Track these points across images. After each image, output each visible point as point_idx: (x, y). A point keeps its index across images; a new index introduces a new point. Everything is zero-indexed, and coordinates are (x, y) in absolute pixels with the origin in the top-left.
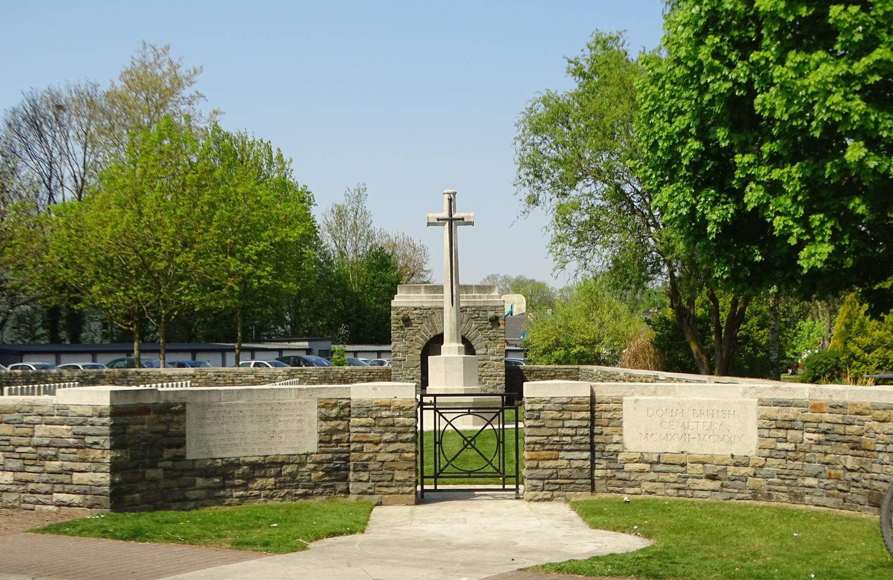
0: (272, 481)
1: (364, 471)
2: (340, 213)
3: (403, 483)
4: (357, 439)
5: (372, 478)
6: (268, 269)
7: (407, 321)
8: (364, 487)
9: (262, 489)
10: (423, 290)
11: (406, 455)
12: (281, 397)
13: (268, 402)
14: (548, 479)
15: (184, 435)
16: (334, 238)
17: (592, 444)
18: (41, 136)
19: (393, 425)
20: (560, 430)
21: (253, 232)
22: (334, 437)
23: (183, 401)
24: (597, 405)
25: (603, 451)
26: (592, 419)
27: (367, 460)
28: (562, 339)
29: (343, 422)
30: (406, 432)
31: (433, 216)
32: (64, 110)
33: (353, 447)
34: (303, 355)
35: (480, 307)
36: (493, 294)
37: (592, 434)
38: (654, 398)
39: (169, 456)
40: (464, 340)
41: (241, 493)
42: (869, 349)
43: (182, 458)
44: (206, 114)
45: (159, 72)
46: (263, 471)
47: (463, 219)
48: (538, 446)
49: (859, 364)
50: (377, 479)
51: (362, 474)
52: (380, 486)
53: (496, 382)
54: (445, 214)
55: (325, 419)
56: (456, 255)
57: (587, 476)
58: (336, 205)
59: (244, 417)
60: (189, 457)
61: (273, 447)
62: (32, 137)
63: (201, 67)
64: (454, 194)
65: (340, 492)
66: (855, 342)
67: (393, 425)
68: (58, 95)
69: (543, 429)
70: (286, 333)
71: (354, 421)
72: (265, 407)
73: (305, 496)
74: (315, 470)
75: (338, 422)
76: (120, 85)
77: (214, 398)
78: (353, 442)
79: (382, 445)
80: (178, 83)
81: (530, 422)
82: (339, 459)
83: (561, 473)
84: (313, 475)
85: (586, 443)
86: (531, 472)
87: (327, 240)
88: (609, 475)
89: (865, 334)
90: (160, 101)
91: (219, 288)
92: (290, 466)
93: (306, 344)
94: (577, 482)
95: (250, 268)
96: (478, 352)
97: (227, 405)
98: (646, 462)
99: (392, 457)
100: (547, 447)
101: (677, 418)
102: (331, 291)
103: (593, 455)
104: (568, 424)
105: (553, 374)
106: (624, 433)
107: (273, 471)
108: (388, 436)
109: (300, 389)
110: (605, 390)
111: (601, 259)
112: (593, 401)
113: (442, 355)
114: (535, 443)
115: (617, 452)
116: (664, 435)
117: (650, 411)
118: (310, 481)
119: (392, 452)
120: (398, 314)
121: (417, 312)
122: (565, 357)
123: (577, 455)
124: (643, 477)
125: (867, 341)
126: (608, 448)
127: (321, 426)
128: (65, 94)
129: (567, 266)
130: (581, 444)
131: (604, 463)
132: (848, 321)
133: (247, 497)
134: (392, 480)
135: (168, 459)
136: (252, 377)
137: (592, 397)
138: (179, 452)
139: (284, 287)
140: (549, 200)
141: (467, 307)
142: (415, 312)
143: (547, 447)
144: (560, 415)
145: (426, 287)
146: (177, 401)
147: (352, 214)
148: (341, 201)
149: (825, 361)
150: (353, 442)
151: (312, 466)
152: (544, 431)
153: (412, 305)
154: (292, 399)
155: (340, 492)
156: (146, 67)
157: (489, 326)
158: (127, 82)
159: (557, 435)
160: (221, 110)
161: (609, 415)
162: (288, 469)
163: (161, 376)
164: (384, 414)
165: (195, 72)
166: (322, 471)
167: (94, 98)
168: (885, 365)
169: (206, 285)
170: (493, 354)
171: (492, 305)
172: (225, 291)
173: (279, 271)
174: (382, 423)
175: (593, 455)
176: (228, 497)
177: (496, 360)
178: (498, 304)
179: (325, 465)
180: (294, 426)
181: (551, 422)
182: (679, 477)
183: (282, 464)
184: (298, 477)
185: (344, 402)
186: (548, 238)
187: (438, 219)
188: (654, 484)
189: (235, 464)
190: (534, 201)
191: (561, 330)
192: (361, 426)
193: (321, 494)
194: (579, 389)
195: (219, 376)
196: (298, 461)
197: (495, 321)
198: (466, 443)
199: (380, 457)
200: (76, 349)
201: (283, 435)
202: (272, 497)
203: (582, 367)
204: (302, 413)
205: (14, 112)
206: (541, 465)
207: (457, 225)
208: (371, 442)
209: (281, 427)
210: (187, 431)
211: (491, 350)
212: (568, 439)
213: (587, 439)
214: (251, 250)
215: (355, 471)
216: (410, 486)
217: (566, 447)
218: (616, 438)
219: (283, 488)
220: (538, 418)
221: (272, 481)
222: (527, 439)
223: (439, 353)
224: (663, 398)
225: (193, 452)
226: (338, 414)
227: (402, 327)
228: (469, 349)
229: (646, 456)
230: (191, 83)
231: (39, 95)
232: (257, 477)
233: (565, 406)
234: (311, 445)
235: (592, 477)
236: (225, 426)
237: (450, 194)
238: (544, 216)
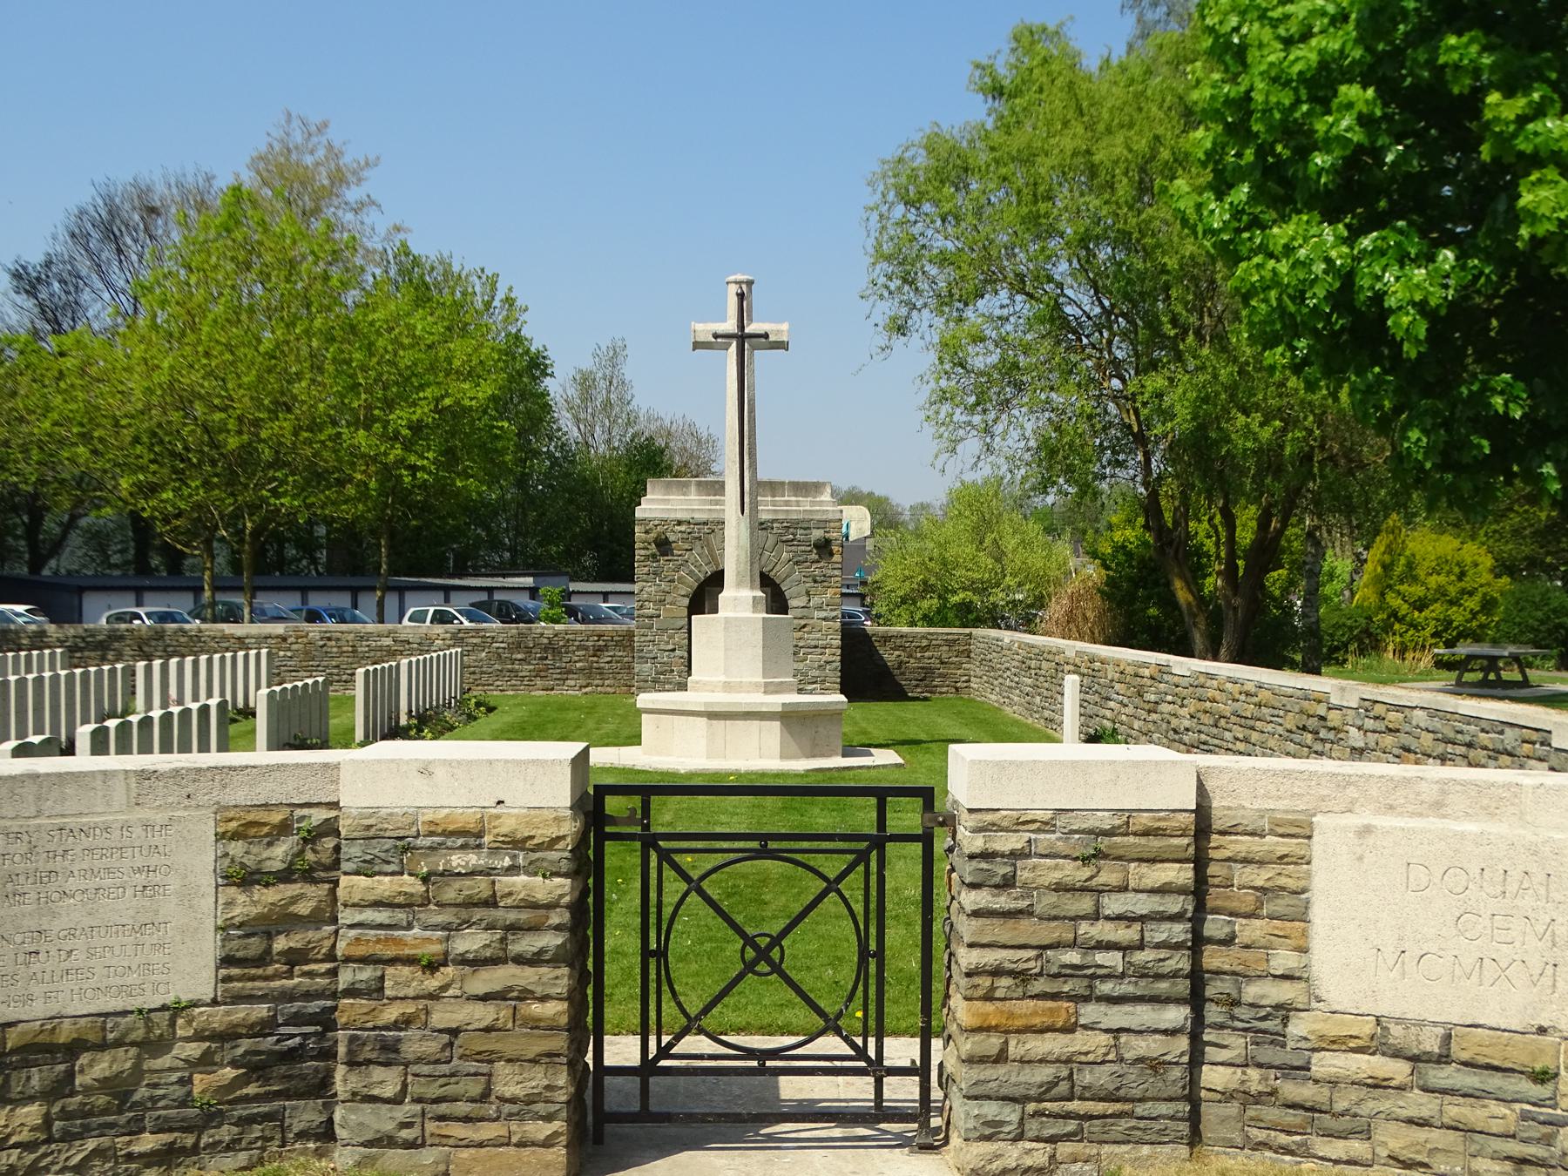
0: (31, 1113)
1: (387, 1064)
2: (585, 383)
3: (525, 1106)
4: (360, 951)
5: (415, 1089)
6: (430, 455)
7: (664, 546)
8: (383, 1120)
10: (693, 488)
11: (536, 1008)
12: (71, 806)
14: (1039, 1100)
16: (578, 421)
17: (1197, 977)
18: (119, 251)
20: (1084, 927)
21: (406, 386)
22: (280, 944)
24: (1216, 839)
25: (1236, 1003)
26: (1199, 889)
27: (395, 1026)
28: (933, 580)
29: (310, 890)
30: (534, 928)
31: (705, 330)
32: (159, 214)
33: (345, 977)
34: (523, 600)
35: (798, 522)
36: (823, 498)
37: (1198, 942)
38: (1433, 823)
40: (767, 582)
42: (1420, 605)
44: (382, 230)
45: (309, 160)
47: (766, 336)
48: (1005, 982)
49: (1404, 628)
50: (434, 1091)
51: (378, 1073)
52: (442, 1118)
53: (824, 658)
54: (730, 326)
55: (247, 878)
56: (752, 410)
57: (1176, 1090)
58: (580, 371)
61: (37, 990)
62: (108, 253)
63: (378, 158)
64: (750, 283)
65: (302, 1135)
66: (1399, 593)
67: (491, 902)
68: (149, 189)
69: (1025, 923)
70: (501, 563)
71: (352, 885)
74: (205, 1062)
76: (248, 179)
78: (348, 959)
79: (450, 970)
80: (339, 178)
81: (982, 899)
82: (297, 1019)
83: (1086, 1077)
84: (200, 1082)
85: (1175, 975)
86: (978, 1073)
87: (565, 422)
88: (1255, 1087)
89: (1415, 579)
90: (309, 205)
91: (341, 483)
92: (106, 1057)
93: (529, 581)
94: (1140, 1110)
95: (398, 451)
96: (792, 603)
98: (1397, 1054)
99: (484, 1014)
100: (1039, 986)
101: (1527, 902)
102: (571, 501)
103: (1198, 1020)
104: (1113, 905)
105: (925, 643)
106: (1317, 944)
107: (36, 1079)
108: (471, 942)
109: (144, 775)
110: (1251, 783)
111: (1021, 430)
112: (1203, 822)
113: (721, 614)
114: (997, 972)
115: (1284, 1011)
116: (1469, 960)
117: (1419, 874)
118: (183, 1103)
119: (485, 998)
120: (647, 532)
121: (683, 528)
122: (939, 611)
123: (1143, 1015)
124: (1385, 1106)
125: (1417, 591)
126: (1251, 992)
127: (230, 904)
128: (160, 189)
129: (959, 448)
130: (1159, 977)
131: (1237, 1045)
132: (1387, 558)
134: (484, 1097)
136: (388, 642)
137: (1202, 812)
139: (459, 484)
140: (929, 325)
141: (773, 521)
142: (678, 528)
143: (1039, 986)
144: (1086, 872)
145: (699, 484)
147: (603, 384)
148: (587, 364)
149: (1349, 623)
150: (348, 959)
151: (194, 1050)
152: (1028, 930)
153: (672, 516)
155: (302, 1135)
156: (289, 150)
157: (814, 556)
158: (258, 172)
159: (1073, 944)
160: (406, 225)
161: (1260, 877)
163: (225, 638)
164: (458, 861)
165: (367, 164)
166: (234, 1064)
167: (206, 197)
168: (1446, 630)
169: (316, 477)
170: (820, 608)
171: (818, 517)
172: (350, 490)
173: (450, 457)
174: (450, 894)
175: (1198, 1020)
177: (824, 619)
178: (830, 517)
179: (245, 1044)
180: (123, 908)
181: (1052, 898)
182: (1525, 1116)
183: (75, 1048)
184: (142, 1093)
185: (318, 816)
186: (926, 392)
187: (716, 336)
188: (1421, 1134)
190: (900, 328)
191: (932, 564)
192: (377, 904)
194: (1151, 778)
195: (329, 639)
196: (138, 1035)
197: (824, 547)
198: (750, 953)
199: (443, 1016)
200: (177, 584)
201: (79, 943)
203: (975, 631)
204: (154, 860)
205: (82, 212)
206: (1014, 1049)
207: (754, 348)
208: (411, 961)
209: (71, 913)
211: (815, 601)
212: (1113, 959)
213: (1181, 962)
214: (400, 418)
215: (352, 1064)
216: (549, 1118)
217: (1106, 988)
218: (1284, 960)
219: (81, 1136)
220: (1007, 883)
221: (31, 1113)
222: (967, 958)
223: (715, 611)
224: (1471, 827)
226: (294, 856)
227: (654, 556)
228: (777, 602)
229: (1396, 1030)
230: (359, 180)
231: (120, 188)
233: (1104, 843)
234: (187, 970)
235: (1192, 1097)
237: (739, 283)
238: (918, 354)
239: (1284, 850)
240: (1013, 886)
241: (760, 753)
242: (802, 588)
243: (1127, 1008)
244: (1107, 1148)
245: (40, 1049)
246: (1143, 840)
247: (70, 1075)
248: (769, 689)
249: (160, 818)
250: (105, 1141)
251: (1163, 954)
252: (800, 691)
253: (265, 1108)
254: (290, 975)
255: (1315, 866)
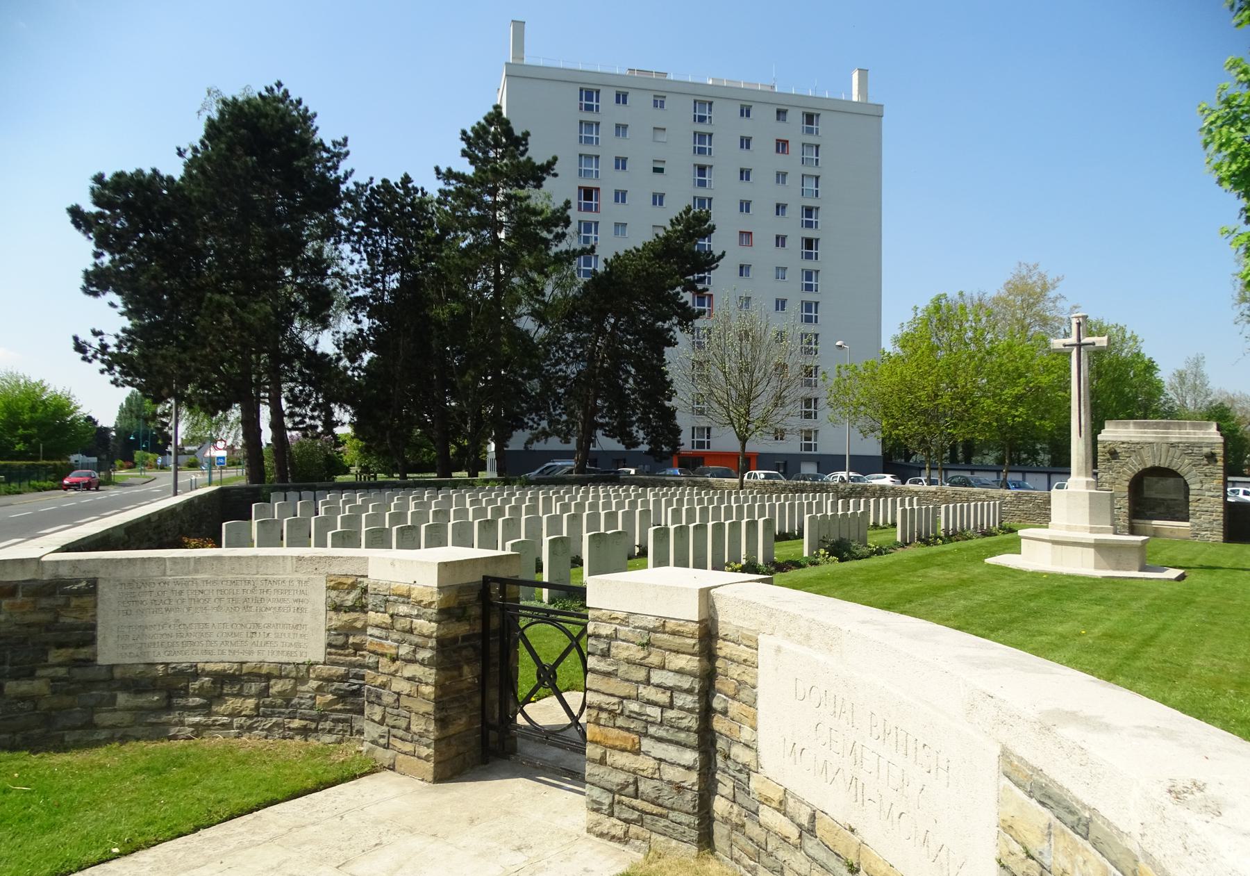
0: (251, 703)
2: (1181, 377)
7: (1114, 454)
9: (233, 715)
13: (248, 577)
15: (93, 627)
19: (411, 631)
23: (91, 576)
39: (60, 659)
41: (197, 719)
43: (90, 662)
46: (238, 687)
48: (604, 715)
55: (337, 608)
59: (206, 600)
60: (102, 660)
61: (255, 649)
72: (242, 586)
73: (304, 732)
75: (354, 615)
77: (154, 571)
80: (1045, 288)
84: (319, 699)
85: (688, 729)
92: (281, 682)
94: (672, 815)
97: (176, 583)
104: (656, 677)
107: (254, 687)
108: (404, 650)
109: (300, 559)
118: (311, 708)
123: (670, 752)
130: (680, 729)
133: (209, 726)
135: (60, 665)
138: (84, 653)
143: (620, 721)
144: (642, 654)
146: (77, 575)
154: (286, 574)
159: (637, 698)
162: (277, 687)
170: (1209, 490)
176: (176, 725)
180: (290, 618)
183: (269, 677)
184: (295, 701)
189: (194, 673)
193: (330, 732)
196: (293, 674)
201: (272, 631)
202: (250, 728)
204: (302, 597)
209: (269, 618)
210: (99, 621)
212: (654, 712)
219: (272, 715)
221: (251, 703)
225: (110, 650)
232: (228, 695)
234: (314, 649)
236: (172, 614)
239: (744, 656)
240: (609, 656)
241: (1083, 565)
242: (1198, 479)
243: (664, 746)
244: (654, 836)
245: (255, 676)
246: (671, 638)
247: (268, 688)
248: (1092, 530)
249: (304, 578)
250: (280, 720)
251: (682, 714)
252: (1115, 533)
253: (343, 716)
254: (355, 654)
255: (759, 671)
